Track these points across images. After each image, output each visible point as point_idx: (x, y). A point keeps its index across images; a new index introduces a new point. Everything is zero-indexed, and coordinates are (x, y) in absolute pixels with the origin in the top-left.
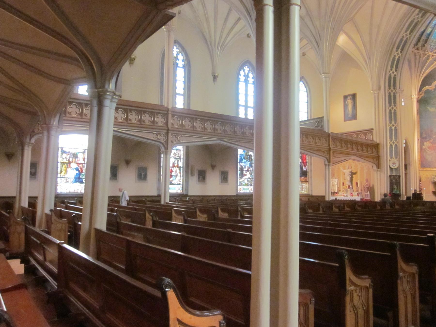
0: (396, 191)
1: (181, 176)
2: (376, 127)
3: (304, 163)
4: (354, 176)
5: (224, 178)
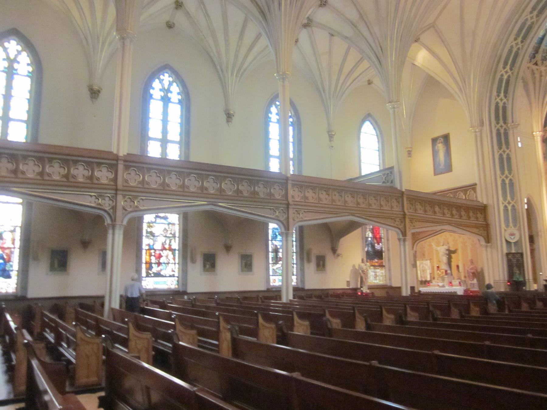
0: (518, 277)
1: (175, 264)
2: (480, 179)
3: (376, 238)
4: (453, 255)
5: (247, 264)
